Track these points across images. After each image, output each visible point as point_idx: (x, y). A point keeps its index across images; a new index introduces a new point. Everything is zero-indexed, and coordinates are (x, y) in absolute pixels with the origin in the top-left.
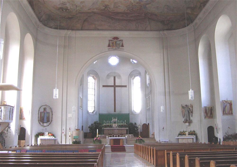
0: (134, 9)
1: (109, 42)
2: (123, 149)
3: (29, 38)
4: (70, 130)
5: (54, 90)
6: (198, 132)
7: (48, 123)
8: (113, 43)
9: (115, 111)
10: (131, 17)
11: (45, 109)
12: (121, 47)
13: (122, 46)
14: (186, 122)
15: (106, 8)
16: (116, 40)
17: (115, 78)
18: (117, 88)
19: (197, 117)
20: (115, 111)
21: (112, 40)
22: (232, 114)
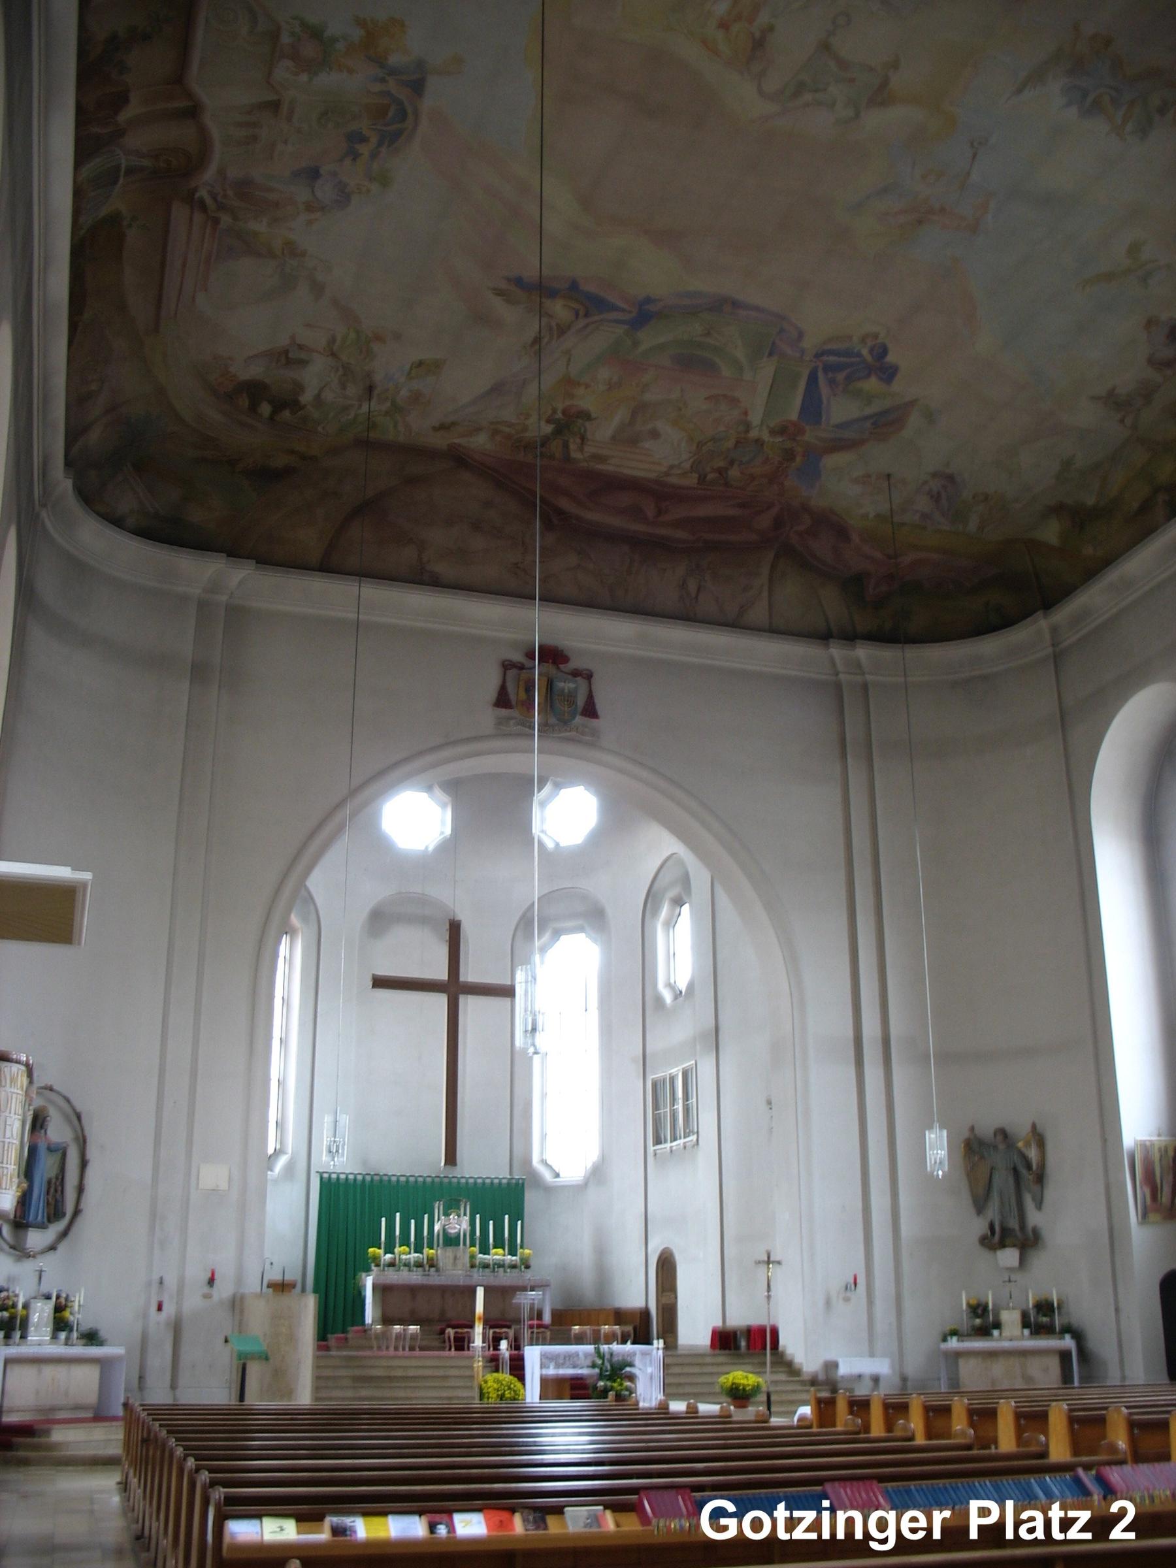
0: (734, 473)
1: (505, 674)
4: (206, 1290)
5: (285, 941)
7: (61, 1225)
9: (451, 1158)
12: (579, 719)
13: (590, 711)
14: (1002, 1245)
15: (558, 432)
18: (440, 1002)
20: (451, 1158)
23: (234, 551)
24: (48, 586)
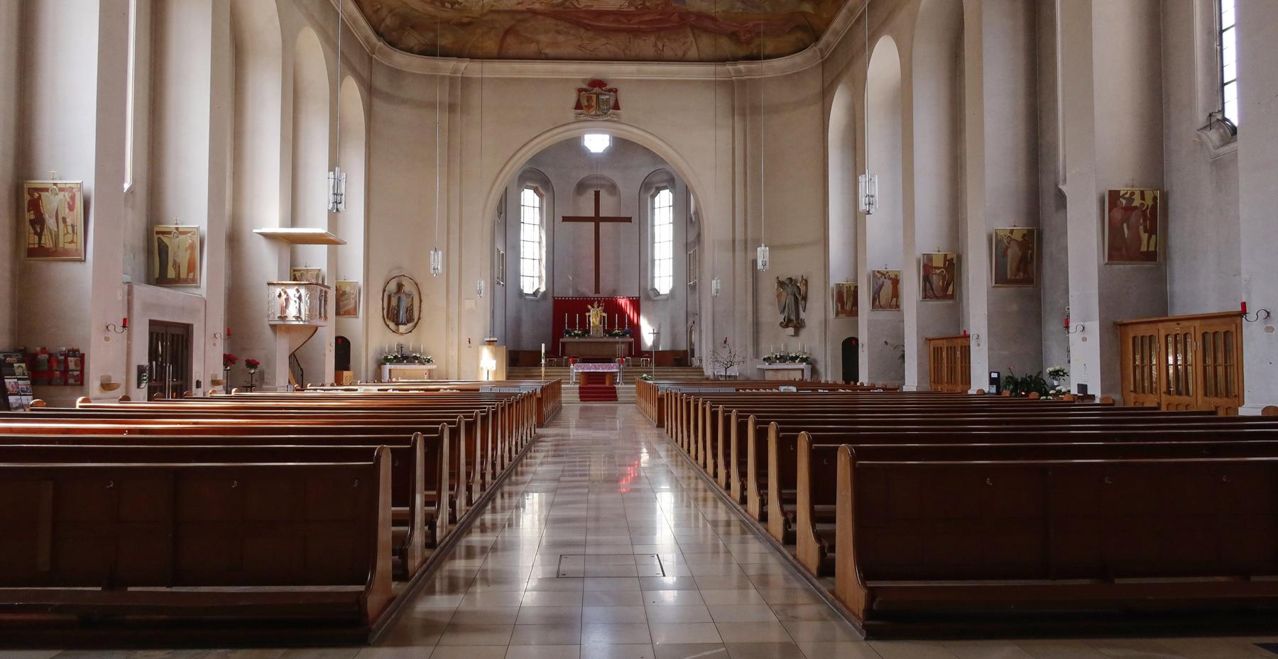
2: (611, 395)
3: (352, 91)
6: (819, 355)
7: (410, 325)
8: (589, 99)
10: (641, 23)
11: (400, 286)
13: (616, 107)
14: (787, 326)
16: (597, 90)
17: (597, 194)
19: (818, 310)
21: (586, 90)
22: (897, 306)
23: (460, 55)
24: (380, 82)
